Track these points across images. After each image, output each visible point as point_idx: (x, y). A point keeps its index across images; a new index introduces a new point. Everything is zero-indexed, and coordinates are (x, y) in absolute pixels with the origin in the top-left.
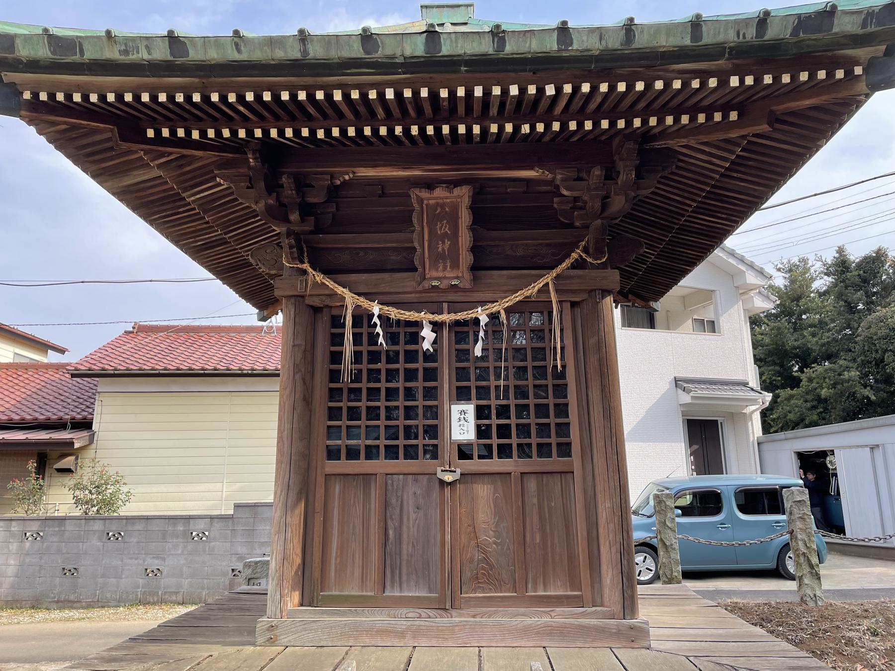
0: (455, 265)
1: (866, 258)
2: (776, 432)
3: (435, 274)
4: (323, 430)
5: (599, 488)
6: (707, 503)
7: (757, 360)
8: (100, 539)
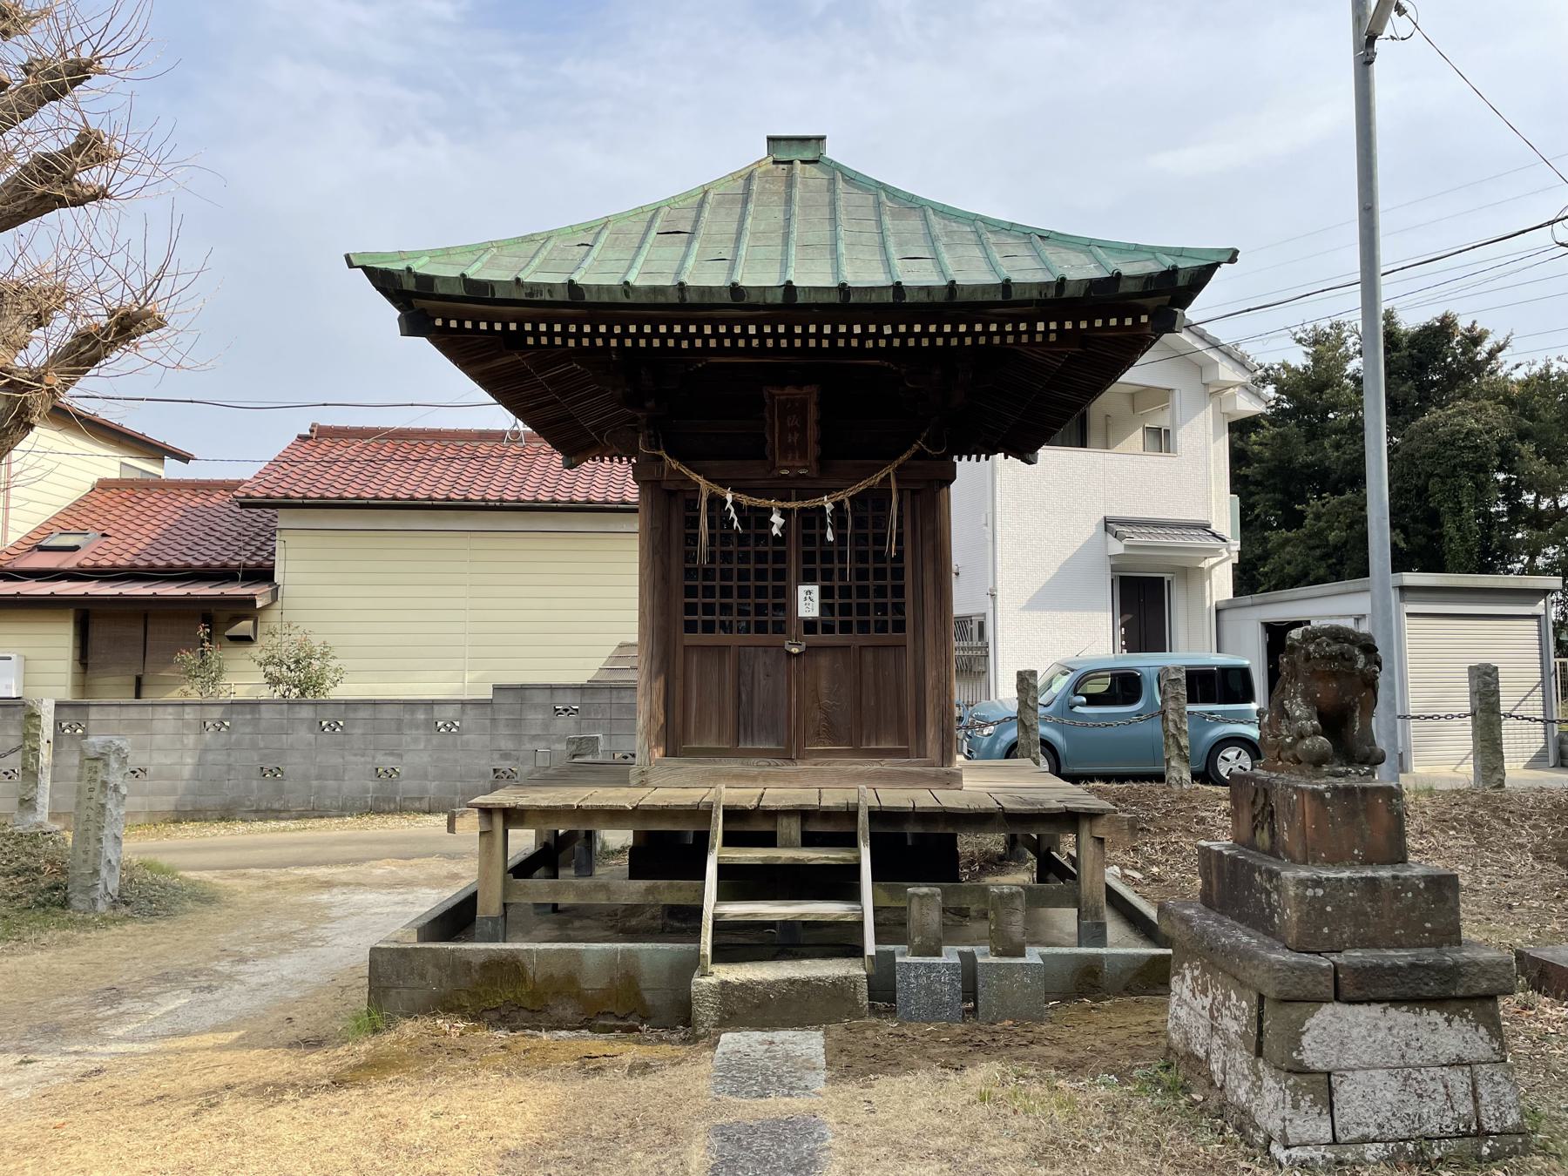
0: (804, 456)
1: (1426, 328)
2: (1268, 590)
3: (785, 463)
4: (681, 607)
5: (928, 659)
6: (1125, 687)
7: (1238, 484)
8: (311, 730)
